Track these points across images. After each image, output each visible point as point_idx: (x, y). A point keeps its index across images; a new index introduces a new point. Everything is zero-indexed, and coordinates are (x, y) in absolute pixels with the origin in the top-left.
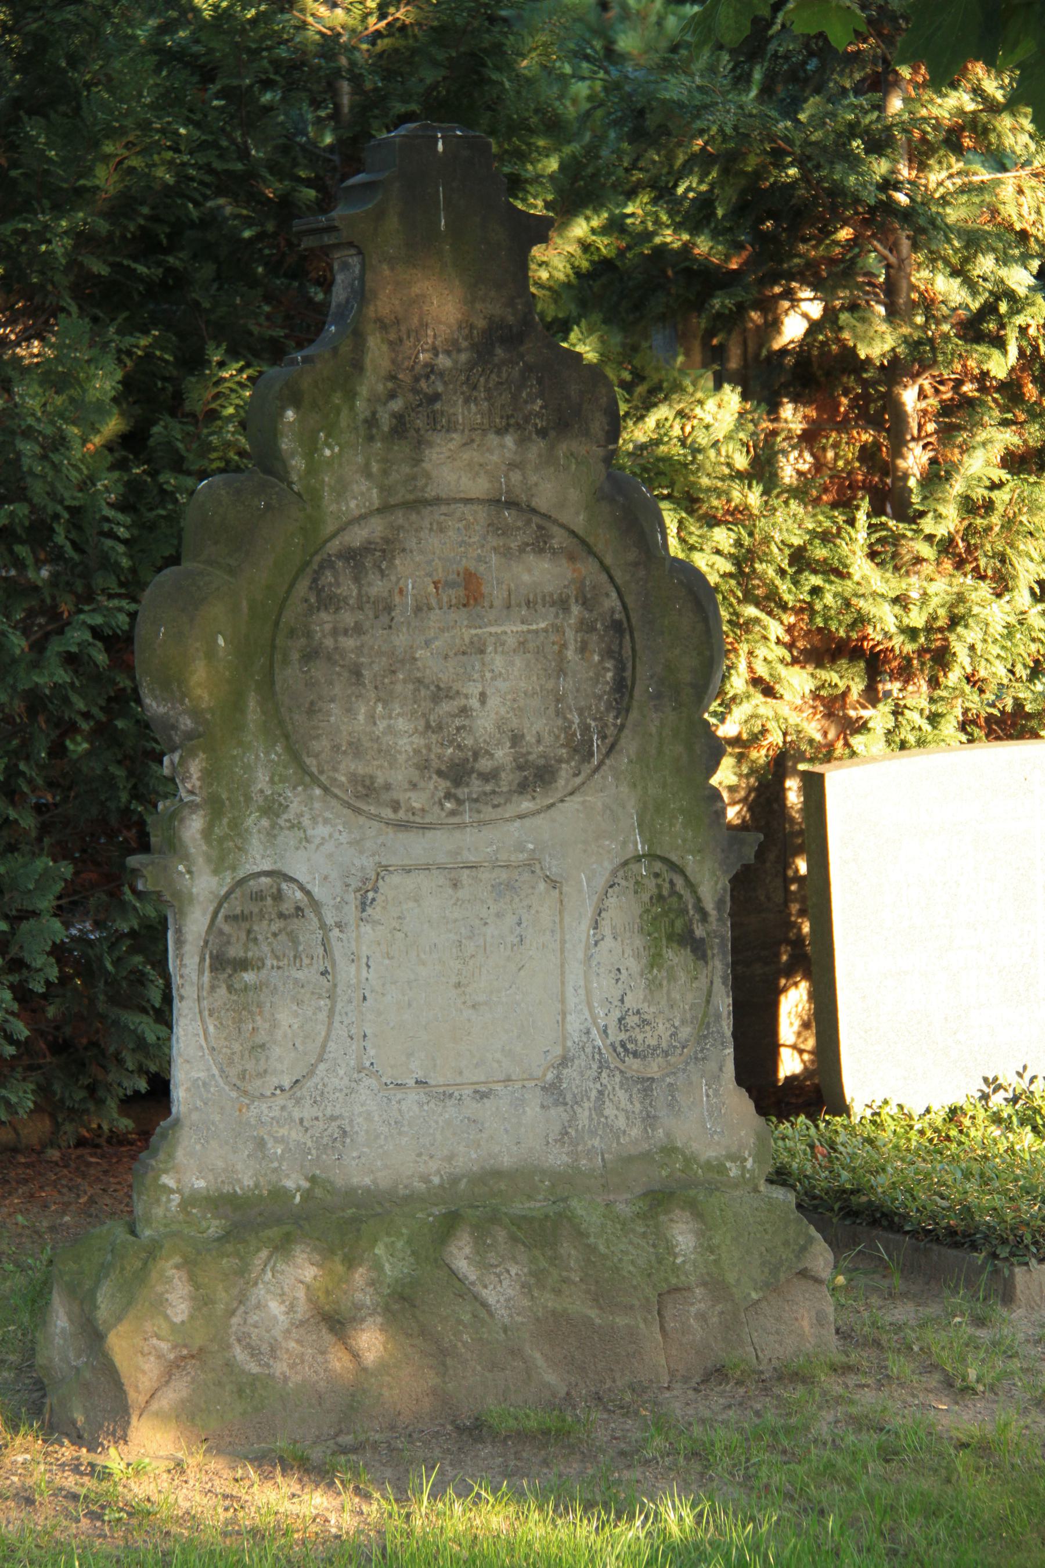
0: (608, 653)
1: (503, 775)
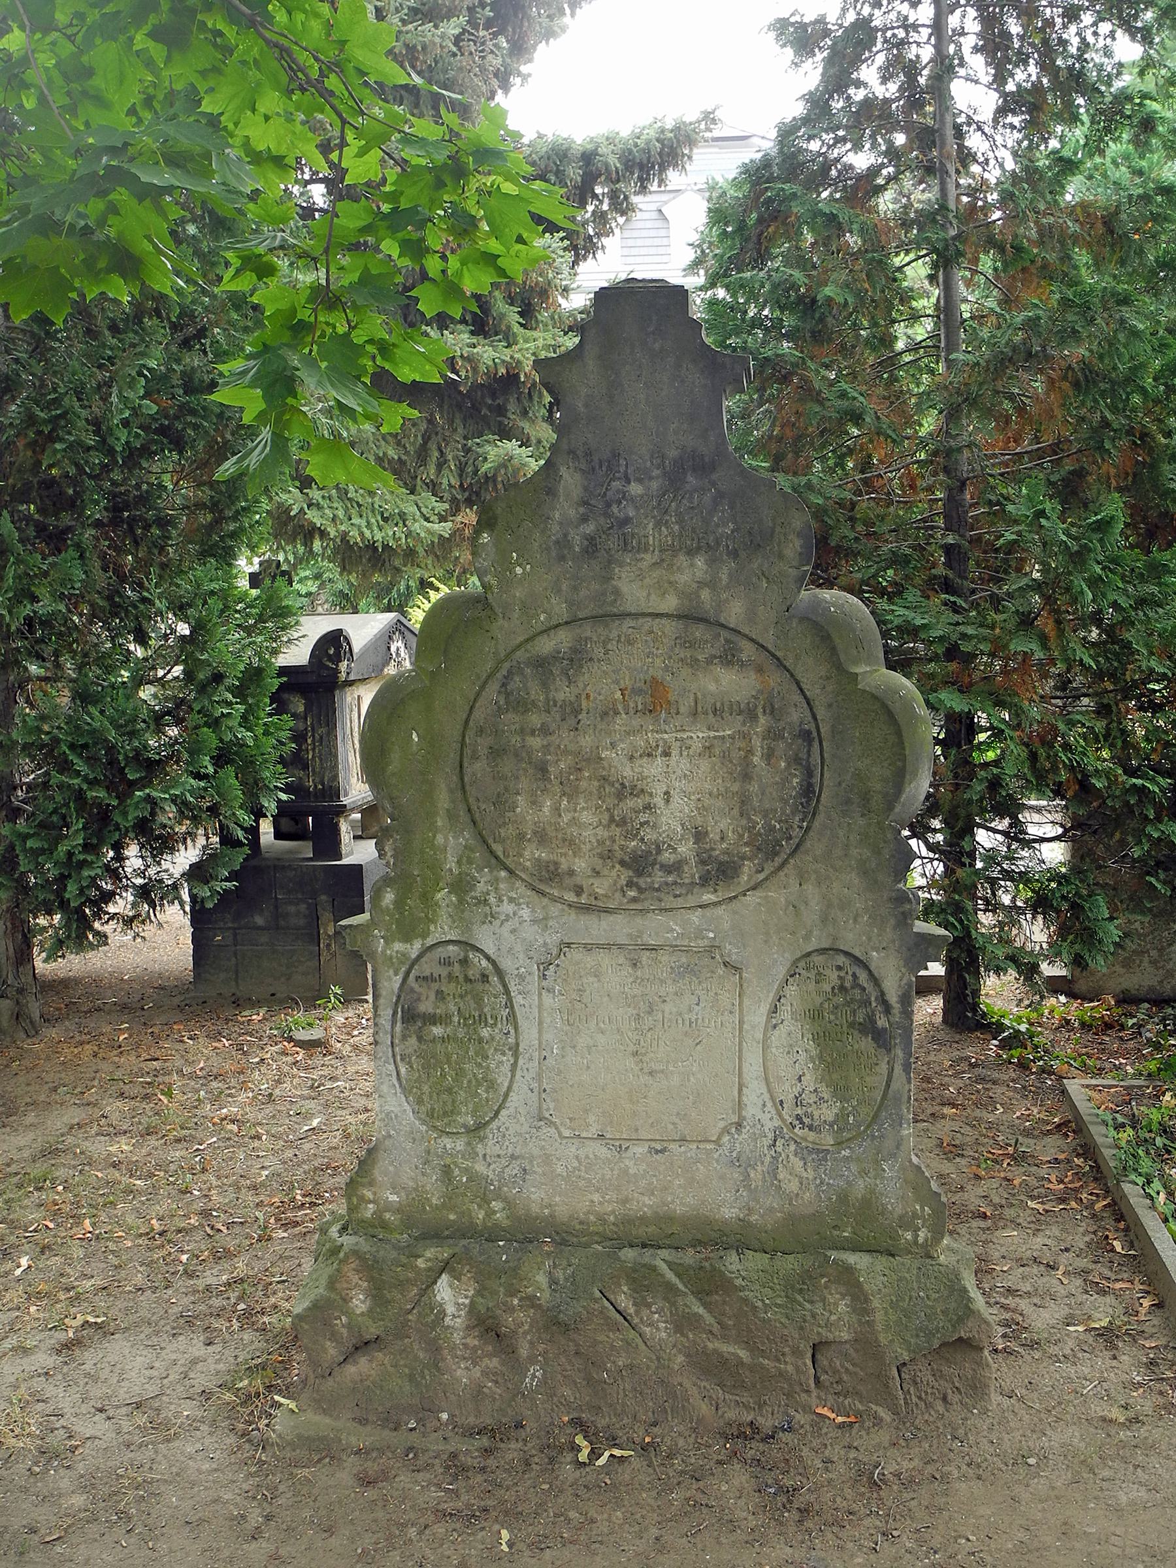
1: (686, 869)
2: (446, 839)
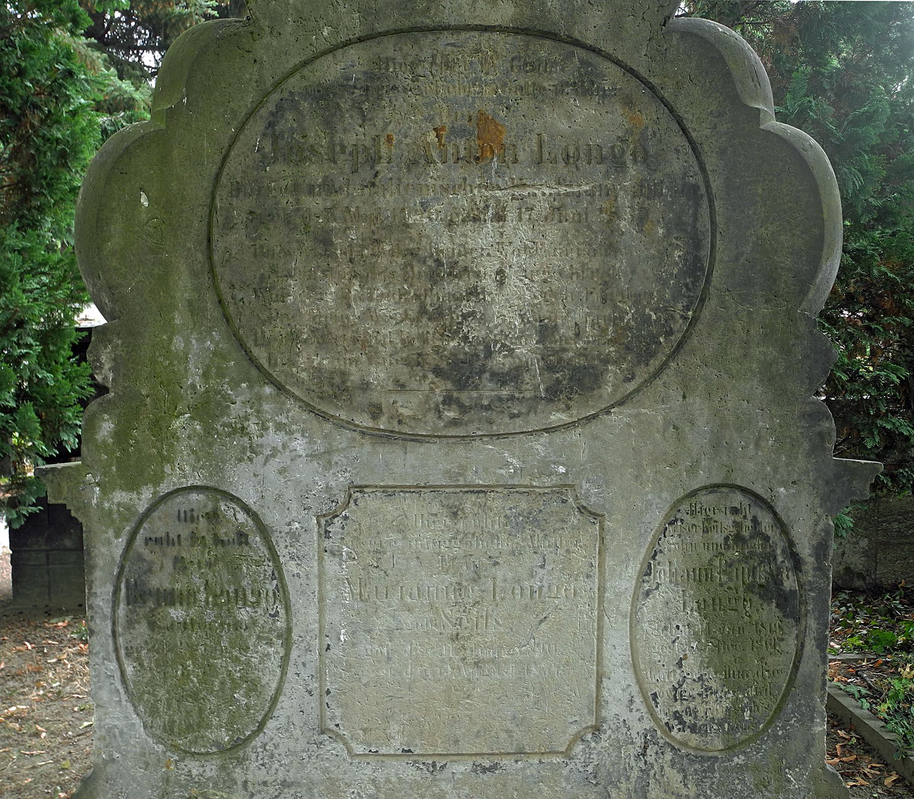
0: (676, 225)
1: (527, 377)
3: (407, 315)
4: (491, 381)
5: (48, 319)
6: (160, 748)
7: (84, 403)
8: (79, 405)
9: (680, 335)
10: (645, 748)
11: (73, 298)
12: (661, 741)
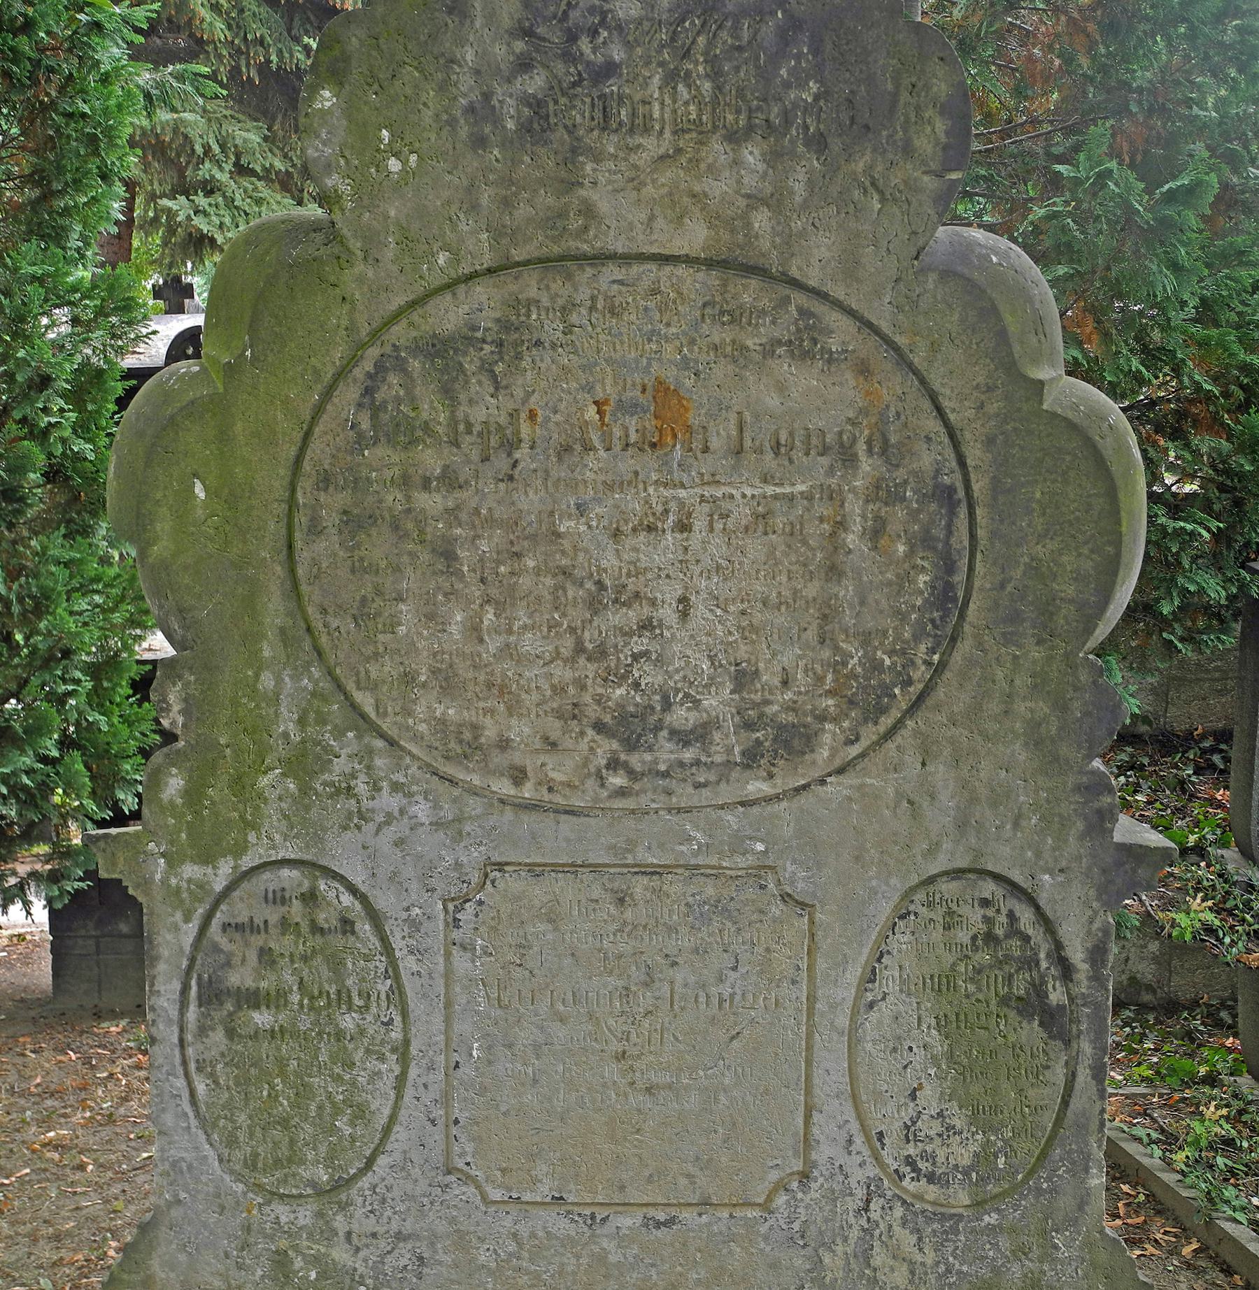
1: (717, 736)
2: (279, 681)
3: (558, 653)
4: (670, 740)
5: (102, 649)
6: (239, 1187)
7: (146, 753)
8: (139, 757)
9: (921, 686)
10: (868, 1201)
11: (133, 622)
12: (889, 1194)
